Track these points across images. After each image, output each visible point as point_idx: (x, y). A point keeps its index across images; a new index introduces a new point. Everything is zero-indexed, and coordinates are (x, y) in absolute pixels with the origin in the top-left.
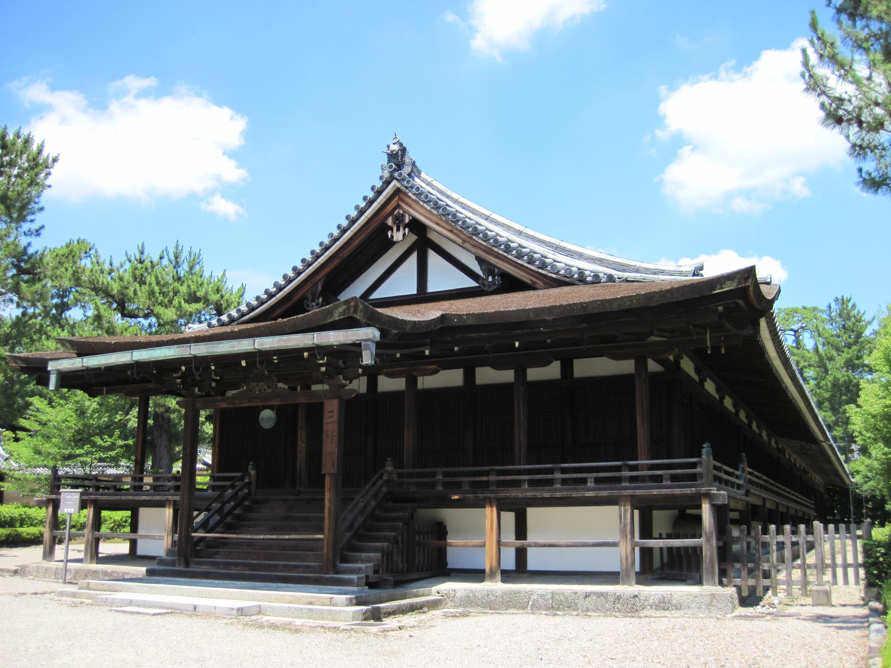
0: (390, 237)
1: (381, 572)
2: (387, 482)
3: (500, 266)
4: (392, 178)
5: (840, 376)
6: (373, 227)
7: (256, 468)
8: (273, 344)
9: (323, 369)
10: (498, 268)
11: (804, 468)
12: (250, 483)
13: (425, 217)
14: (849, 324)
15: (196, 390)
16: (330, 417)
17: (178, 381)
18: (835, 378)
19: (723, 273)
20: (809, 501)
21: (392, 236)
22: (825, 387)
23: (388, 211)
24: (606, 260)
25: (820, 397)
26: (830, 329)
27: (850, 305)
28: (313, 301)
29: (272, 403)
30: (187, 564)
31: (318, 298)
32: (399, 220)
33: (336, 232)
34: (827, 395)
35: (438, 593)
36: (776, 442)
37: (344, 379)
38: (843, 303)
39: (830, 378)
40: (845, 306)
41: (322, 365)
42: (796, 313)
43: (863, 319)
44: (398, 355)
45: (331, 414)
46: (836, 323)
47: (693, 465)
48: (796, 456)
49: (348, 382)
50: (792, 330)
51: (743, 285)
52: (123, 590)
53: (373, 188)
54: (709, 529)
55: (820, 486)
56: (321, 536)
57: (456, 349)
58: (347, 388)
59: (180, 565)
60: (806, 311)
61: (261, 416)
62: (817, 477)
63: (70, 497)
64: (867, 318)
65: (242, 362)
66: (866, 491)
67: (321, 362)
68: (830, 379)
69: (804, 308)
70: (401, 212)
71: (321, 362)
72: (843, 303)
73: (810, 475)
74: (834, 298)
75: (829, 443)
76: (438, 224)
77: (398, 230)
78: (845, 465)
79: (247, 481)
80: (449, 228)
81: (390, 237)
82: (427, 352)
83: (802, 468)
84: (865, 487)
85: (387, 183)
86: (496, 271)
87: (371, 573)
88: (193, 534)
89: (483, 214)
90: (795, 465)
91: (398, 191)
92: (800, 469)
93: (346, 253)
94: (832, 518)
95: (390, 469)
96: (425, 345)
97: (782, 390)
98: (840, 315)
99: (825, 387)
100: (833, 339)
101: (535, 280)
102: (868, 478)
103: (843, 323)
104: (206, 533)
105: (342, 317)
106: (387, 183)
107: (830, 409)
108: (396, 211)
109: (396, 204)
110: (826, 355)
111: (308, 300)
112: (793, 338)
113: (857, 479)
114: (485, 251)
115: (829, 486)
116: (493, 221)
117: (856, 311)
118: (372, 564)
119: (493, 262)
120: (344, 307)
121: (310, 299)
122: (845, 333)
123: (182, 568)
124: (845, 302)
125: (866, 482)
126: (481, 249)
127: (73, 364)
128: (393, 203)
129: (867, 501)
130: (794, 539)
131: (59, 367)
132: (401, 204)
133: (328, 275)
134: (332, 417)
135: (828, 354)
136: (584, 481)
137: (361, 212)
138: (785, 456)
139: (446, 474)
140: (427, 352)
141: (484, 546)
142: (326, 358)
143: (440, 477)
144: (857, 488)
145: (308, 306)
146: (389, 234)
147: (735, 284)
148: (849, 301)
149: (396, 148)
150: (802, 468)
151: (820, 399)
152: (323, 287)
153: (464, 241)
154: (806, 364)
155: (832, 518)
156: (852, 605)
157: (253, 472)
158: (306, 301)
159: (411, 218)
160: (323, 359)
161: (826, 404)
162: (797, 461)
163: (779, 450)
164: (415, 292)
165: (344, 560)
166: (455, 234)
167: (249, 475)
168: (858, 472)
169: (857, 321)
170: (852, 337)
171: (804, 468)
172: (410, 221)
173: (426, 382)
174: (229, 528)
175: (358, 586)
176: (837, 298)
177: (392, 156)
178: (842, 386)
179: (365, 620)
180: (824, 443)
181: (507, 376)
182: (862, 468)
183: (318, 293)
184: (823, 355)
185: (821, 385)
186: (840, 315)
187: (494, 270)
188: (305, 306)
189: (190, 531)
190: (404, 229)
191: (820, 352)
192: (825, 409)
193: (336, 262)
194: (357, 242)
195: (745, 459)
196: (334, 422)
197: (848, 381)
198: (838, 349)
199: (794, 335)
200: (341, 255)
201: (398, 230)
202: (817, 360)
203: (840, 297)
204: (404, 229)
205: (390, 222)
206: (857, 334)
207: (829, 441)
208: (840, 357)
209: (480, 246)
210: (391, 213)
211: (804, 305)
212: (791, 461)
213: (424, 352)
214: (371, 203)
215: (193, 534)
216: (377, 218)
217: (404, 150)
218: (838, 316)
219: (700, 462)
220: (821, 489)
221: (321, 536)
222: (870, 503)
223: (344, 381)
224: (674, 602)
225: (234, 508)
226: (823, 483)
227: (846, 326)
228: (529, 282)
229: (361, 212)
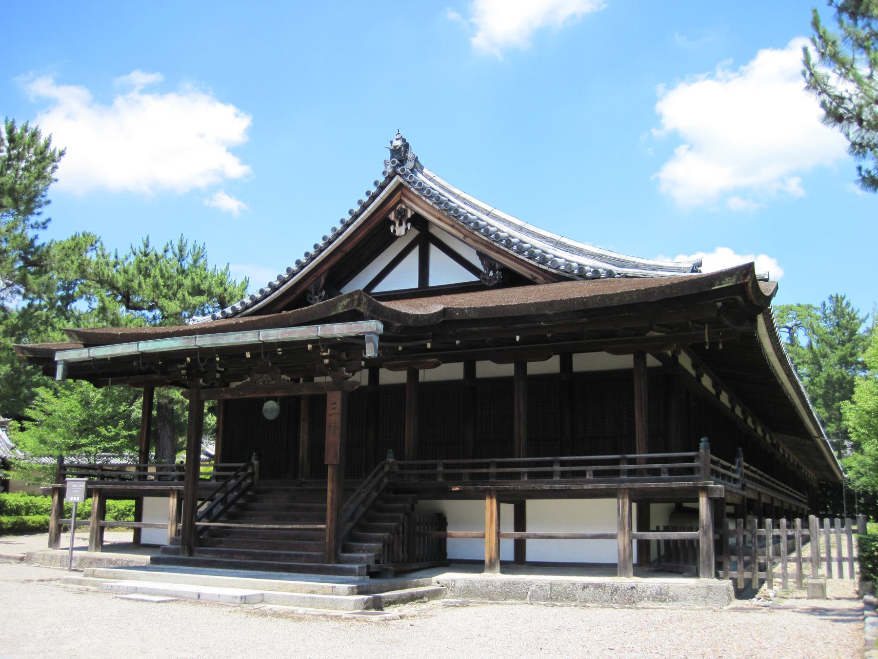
0: (392, 231)
1: (381, 562)
2: (388, 473)
3: (501, 261)
4: (395, 173)
6: (376, 221)
7: (259, 458)
8: (278, 336)
9: (327, 361)
10: (499, 263)
11: (798, 464)
12: (252, 474)
13: (427, 212)
14: (843, 321)
15: (201, 381)
16: (332, 409)
17: (183, 372)
20: (802, 496)
21: (395, 231)
22: (818, 384)
23: (391, 206)
24: (606, 256)
25: (813, 394)
26: (824, 327)
27: (844, 303)
28: (316, 294)
29: (276, 395)
30: (191, 553)
31: (321, 292)
32: (401, 215)
33: (339, 227)
34: (821, 392)
35: (438, 583)
36: (771, 438)
37: (347, 372)
39: (824, 375)
40: (839, 304)
41: (325, 357)
43: (857, 316)
44: (400, 348)
45: (334, 406)
46: (830, 320)
47: (691, 459)
48: (789, 452)
49: (351, 374)
50: (786, 327)
51: (742, 281)
52: (128, 578)
53: (376, 183)
54: (706, 523)
56: (323, 526)
57: (458, 342)
58: (349, 380)
59: (183, 553)
61: (265, 407)
62: (810, 472)
63: (76, 486)
64: (861, 315)
65: (247, 353)
66: (858, 487)
67: (325, 354)
68: (824, 376)
69: (799, 305)
70: (404, 207)
71: (325, 354)
72: (837, 301)
76: (440, 219)
77: (400, 224)
78: (838, 461)
79: (250, 471)
80: (451, 223)
81: (392, 231)
82: (429, 346)
83: (796, 463)
84: (857, 483)
85: (390, 178)
86: (497, 266)
87: (372, 563)
88: (197, 523)
89: (484, 209)
91: (400, 186)
92: (794, 464)
93: (348, 248)
94: (824, 513)
95: (391, 460)
96: (427, 338)
98: (834, 313)
99: (818, 384)
100: (827, 336)
101: (535, 275)
102: (860, 473)
104: (210, 522)
105: (346, 310)
106: (390, 178)
107: (823, 405)
108: (399, 206)
109: (398, 199)
111: (311, 293)
113: (849, 475)
114: (486, 246)
115: (822, 482)
116: (494, 217)
117: (850, 309)
118: (374, 554)
119: (493, 257)
120: (348, 300)
121: (313, 292)
123: (186, 557)
124: (839, 300)
125: (858, 478)
126: (482, 244)
127: (80, 354)
128: (396, 198)
129: (859, 497)
130: (790, 533)
131: (66, 358)
132: (403, 198)
133: (331, 268)
134: (335, 408)
135: (822, 351)
136: (583, 474)
137: (364, 207)
138: (779, 451)
139: (446, 466)
140: (429, 346)
141: (484, 537)
142: (329, 350)
143: (440, 469)
144: (850, 484)
145: (311, 299)
146: (392, 228)
147: (734, 280)
148: (843, 299)
149: (399, 143)
150: (796, 463)
152: (326, 280)
153: (465, 236)
154: (800, 361)
155: (824, 513)
157: (256, 463)
158: (309, 294)
159: (413, 213)
160: (327, 352)
161: (820, 401)
163: (773, 445)
164: (417, 286)
165: (346, 550)
166: (457, 229)
167: (253, 465)
168: (850, 468)
169: (850, 318)
171: (798, 464)
172: (412, 216)
173: (427, 375)
174: (232, 518)
175: (359, 575)
176: (831, 296)
177: (395, 152)
178: (836, 382)
179: (366, 609)
181: (507, 369)
182: (854, 464)
183: (321, 287)
184: (817, 352)
186: (834, 313)
187: (495, 265)
188: (308, 300)
189: (194, 519)
190: (406, 224)
191: (814, 349)
192: (818, 405)
193: (339, 256)
194: (360, 236)
196: (337, 414)
197: (841, 377)
198: (832, 347)
199: (789, 332)
200: (344, 249)
201: (400, 224)
203: (834, 295)
204: (406, 224)
205: (392, 216)
208: (834, 354)
209: (481, 241)
210: (393, 208)
211: (798, 302)
213: (426, 345)
214: (373, 198)
215: (197, 523)
216: (377, 215)
217: (406, 146)
219: (698, 456)
221: (323, 526)
222: (862, 499)
223: (347, 374)
224: (671, 594)
225: (237, 498)
226: (816, 478)
227: (840, 323)
228: (530, 277)
229: (364, 207)
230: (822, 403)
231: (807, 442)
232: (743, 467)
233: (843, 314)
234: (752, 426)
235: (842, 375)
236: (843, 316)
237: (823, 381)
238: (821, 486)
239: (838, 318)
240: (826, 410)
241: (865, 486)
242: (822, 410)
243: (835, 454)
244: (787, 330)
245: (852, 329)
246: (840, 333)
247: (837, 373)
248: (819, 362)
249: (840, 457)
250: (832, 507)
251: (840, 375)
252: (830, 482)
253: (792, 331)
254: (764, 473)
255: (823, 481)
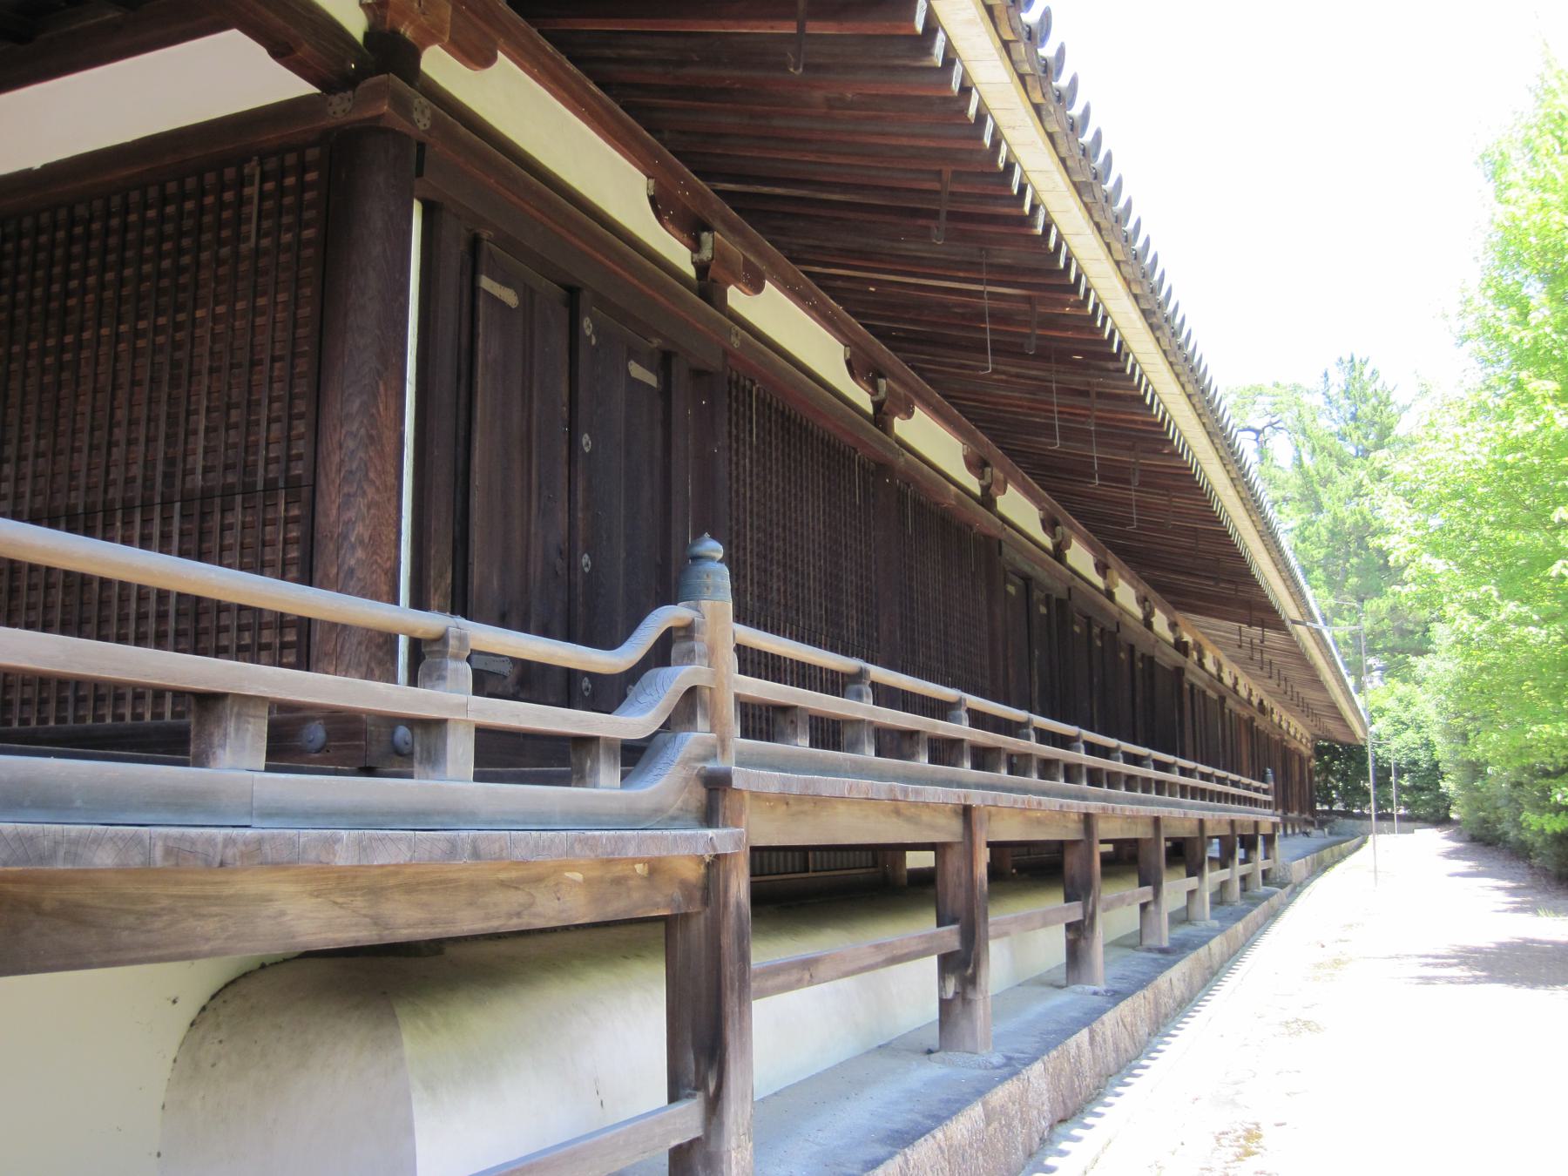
5: (1346, 514)
11: (1261, 702)
14: (1365, 410)
18: (1335, 518)
19: (1529, 990)
20: (1256, 784)
22: (1314, 539)
25: (1305, 559)
27: (1367, 372)
34: (1319, 554)
36: (1173, 626)
38: (1353, 368)
39: (1325, 519)
40: (1356, 374)
42: (1260, 394)
43: (1392, 399)
46: (1338, 408)
48: (1237, 671)
50: (1249, 429)
55: (1301, 742)
60: (1278, 391)
62: (1294, 722)
64: (1400, 398)
66: (1398, 751)
68: (1325, 521)
72: (1353, 368)
73: (1276, 718)
74: (1336, 360)
75: (1315, 626)
83: (1255, 701)
84: (1396, 743)
90: (1236, 691)
92: (1250, 702)
97: (1185, 481)
99: (1314, 539)
100: (1332, 440)
102: (1403, 723)
103: (1353, 409)
107: (1325, 582)
110: (1318, 474)
112: (1255, 445)
113: (1381, 726)
115: (1321, 743)
117: (1378, 385)
122: (1357, 428)
125: (1397, 733)
135: (1321, 471)
144: (1380, 746)
150: (1255, 701)
151: (1305, 563)
154: (1278, 494)
156: (1375, 853)
161: (1318, 573)
162: (1254, 693)
163: (1181, 646)
168: (1381, 711)
169: (1380, 403)
170: (1371, 437)
171: (1261, 702)
178: (1350, 534)
180: (1298, 627)
182: (1390, 703)
184: (1313, 472)
185: (1307, 533)
186: (1347, 394)
191: (1305, 466)
192: (1314, 583)
195: (721, 577)
197: (1361, 523)
198: (1342, 463)
199: (1256, 440)
202: (1299, 482)
203: (1347, 358)
206: (1381, 430)
207: (1315, 621)
208: (1346, 477)
212: (1220, 679)
218: (1342, 395)
220: (1302, 748)
222: (1406, 776)
226: (1308, 735)
227: (1359, 413)
230: (1323, 578)
231: (1270, 634)
232: (732, 660)
233: (1365, 395)
234: (1098, 581)
235: (1364, 518)
236: (1365, 400)
237: (1324, 534)
238: (1319, 752)
239: (1355, 405)
240: (1330, 592)
241: (1412, 750)
242: (1323, 591)
243: (1350, 682)
244: (1253, 436)
245: (1382, 423)
246: (1359, 433)
247: (1353, 513)
248: (1315, 493)
249: (1360, 688)
250: (1344, 796)
251: (1359, 517)
252: (1338, 743)
253: (1261, 437)
254: (1081, 727)
255: (1325, 740)
